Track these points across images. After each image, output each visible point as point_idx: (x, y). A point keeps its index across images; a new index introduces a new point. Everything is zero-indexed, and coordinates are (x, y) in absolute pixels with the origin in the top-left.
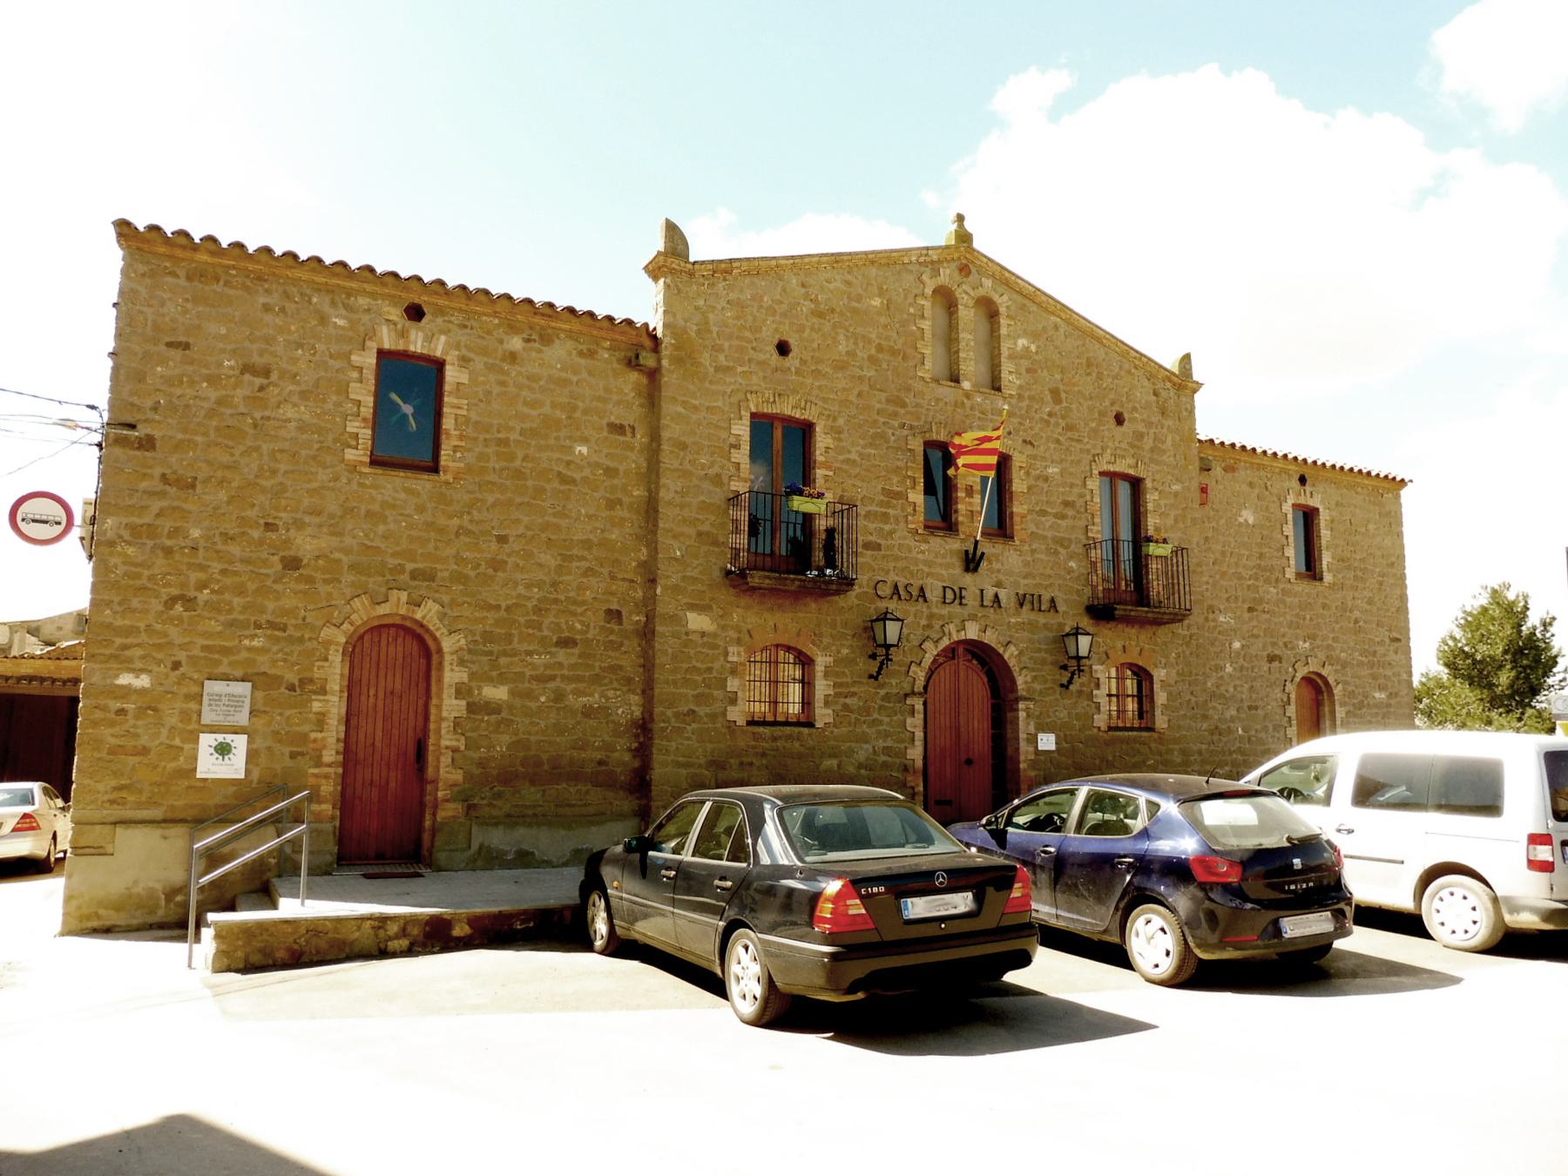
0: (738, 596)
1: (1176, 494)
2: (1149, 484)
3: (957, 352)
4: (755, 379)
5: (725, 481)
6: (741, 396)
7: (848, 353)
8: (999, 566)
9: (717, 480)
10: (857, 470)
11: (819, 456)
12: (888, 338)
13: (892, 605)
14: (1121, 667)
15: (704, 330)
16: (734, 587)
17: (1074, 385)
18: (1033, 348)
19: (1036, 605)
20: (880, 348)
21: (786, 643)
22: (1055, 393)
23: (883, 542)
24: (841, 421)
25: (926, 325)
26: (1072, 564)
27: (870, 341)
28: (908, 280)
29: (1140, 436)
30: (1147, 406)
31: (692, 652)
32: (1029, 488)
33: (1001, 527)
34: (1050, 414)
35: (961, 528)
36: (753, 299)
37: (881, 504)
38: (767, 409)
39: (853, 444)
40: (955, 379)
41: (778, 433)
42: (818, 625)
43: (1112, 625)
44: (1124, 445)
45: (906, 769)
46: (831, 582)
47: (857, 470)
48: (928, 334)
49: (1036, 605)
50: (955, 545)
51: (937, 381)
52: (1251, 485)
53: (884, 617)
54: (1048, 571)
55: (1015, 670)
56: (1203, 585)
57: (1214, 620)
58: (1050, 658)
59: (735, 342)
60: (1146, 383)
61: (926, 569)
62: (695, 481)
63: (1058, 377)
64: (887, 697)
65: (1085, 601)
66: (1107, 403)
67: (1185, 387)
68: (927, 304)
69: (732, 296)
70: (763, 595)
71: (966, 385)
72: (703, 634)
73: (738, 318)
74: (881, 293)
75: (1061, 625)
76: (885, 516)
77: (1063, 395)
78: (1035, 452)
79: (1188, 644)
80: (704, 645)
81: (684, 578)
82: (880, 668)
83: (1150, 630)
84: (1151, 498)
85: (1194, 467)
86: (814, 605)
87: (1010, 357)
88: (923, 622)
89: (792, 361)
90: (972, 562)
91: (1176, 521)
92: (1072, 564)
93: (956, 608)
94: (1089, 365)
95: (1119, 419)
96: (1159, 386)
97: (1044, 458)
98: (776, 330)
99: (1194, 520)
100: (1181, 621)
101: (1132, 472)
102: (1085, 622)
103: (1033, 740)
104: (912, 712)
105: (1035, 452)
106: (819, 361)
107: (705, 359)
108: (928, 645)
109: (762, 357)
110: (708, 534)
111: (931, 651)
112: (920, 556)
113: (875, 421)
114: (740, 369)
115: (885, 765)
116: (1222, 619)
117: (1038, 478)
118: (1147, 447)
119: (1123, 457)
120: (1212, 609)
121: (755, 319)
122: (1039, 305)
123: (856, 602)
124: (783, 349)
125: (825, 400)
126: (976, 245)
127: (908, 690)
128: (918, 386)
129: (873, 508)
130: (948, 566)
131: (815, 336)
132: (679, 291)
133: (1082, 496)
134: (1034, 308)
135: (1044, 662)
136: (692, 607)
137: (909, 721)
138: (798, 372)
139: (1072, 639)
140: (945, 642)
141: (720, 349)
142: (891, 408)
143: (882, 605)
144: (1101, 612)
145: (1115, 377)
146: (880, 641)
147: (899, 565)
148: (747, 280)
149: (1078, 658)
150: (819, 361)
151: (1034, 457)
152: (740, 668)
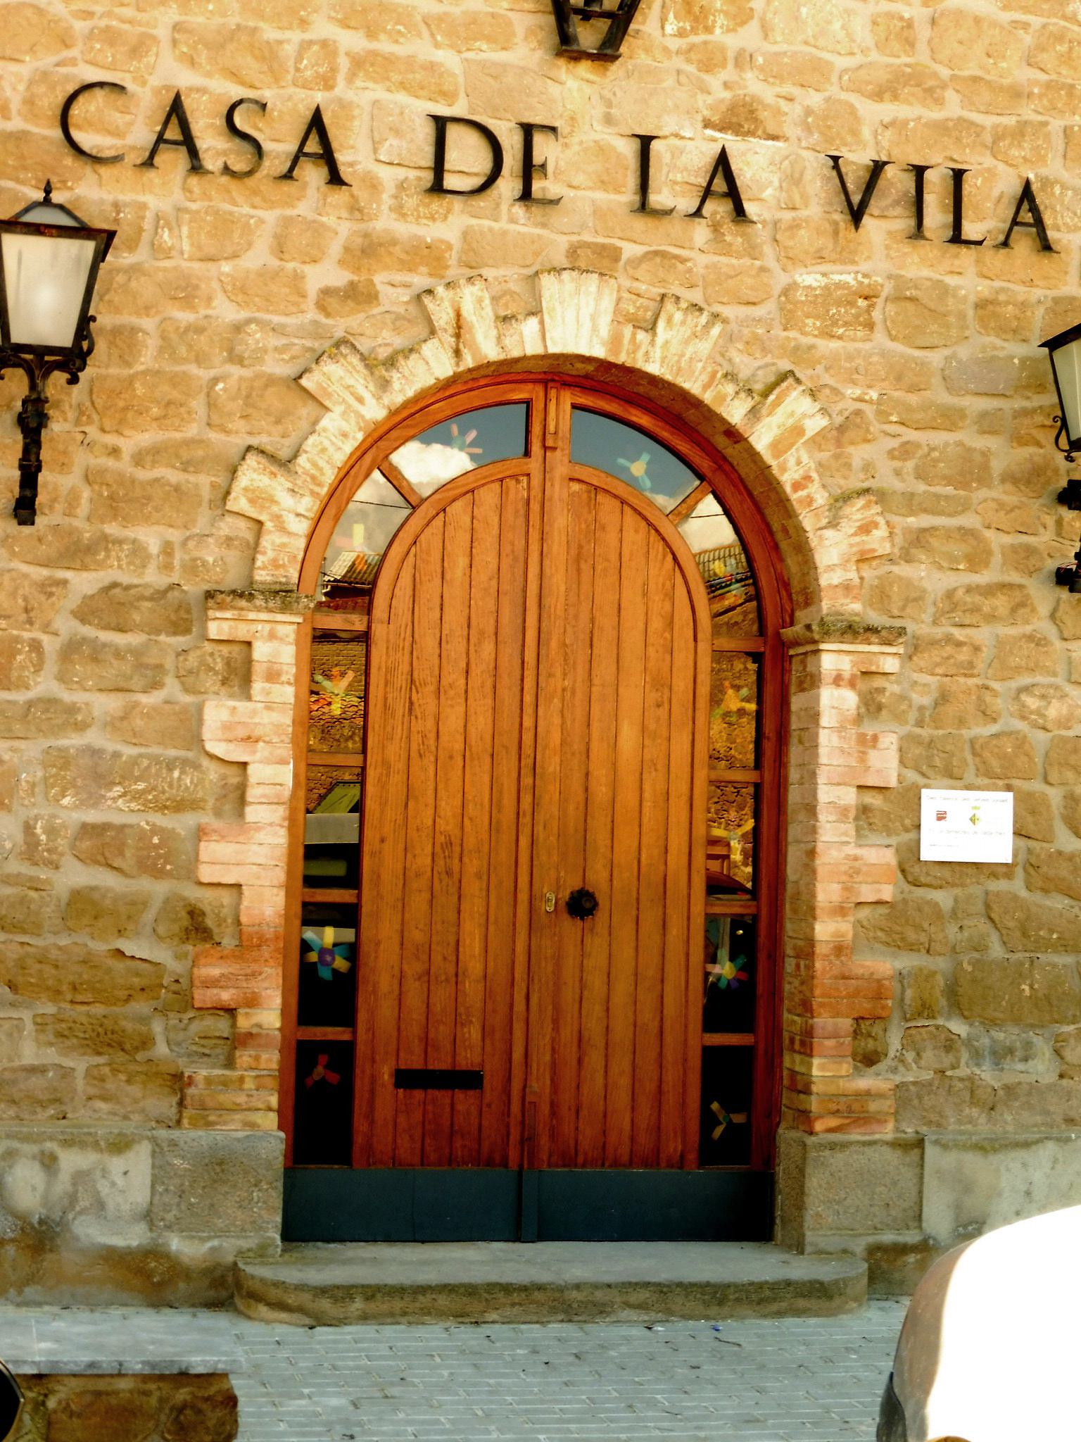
8: (748, 37)
19: (936, 215)
45: (196, 927)
49: (936, 215)
58: (1004, 455)
64: (110, 607)
88: (326, 274)
93: (503, 213)
103: (891, 812)
104: (240, 673)
108: (338, 377)
115: (83, 907)
135: (972, 471)
137: (218, 712)
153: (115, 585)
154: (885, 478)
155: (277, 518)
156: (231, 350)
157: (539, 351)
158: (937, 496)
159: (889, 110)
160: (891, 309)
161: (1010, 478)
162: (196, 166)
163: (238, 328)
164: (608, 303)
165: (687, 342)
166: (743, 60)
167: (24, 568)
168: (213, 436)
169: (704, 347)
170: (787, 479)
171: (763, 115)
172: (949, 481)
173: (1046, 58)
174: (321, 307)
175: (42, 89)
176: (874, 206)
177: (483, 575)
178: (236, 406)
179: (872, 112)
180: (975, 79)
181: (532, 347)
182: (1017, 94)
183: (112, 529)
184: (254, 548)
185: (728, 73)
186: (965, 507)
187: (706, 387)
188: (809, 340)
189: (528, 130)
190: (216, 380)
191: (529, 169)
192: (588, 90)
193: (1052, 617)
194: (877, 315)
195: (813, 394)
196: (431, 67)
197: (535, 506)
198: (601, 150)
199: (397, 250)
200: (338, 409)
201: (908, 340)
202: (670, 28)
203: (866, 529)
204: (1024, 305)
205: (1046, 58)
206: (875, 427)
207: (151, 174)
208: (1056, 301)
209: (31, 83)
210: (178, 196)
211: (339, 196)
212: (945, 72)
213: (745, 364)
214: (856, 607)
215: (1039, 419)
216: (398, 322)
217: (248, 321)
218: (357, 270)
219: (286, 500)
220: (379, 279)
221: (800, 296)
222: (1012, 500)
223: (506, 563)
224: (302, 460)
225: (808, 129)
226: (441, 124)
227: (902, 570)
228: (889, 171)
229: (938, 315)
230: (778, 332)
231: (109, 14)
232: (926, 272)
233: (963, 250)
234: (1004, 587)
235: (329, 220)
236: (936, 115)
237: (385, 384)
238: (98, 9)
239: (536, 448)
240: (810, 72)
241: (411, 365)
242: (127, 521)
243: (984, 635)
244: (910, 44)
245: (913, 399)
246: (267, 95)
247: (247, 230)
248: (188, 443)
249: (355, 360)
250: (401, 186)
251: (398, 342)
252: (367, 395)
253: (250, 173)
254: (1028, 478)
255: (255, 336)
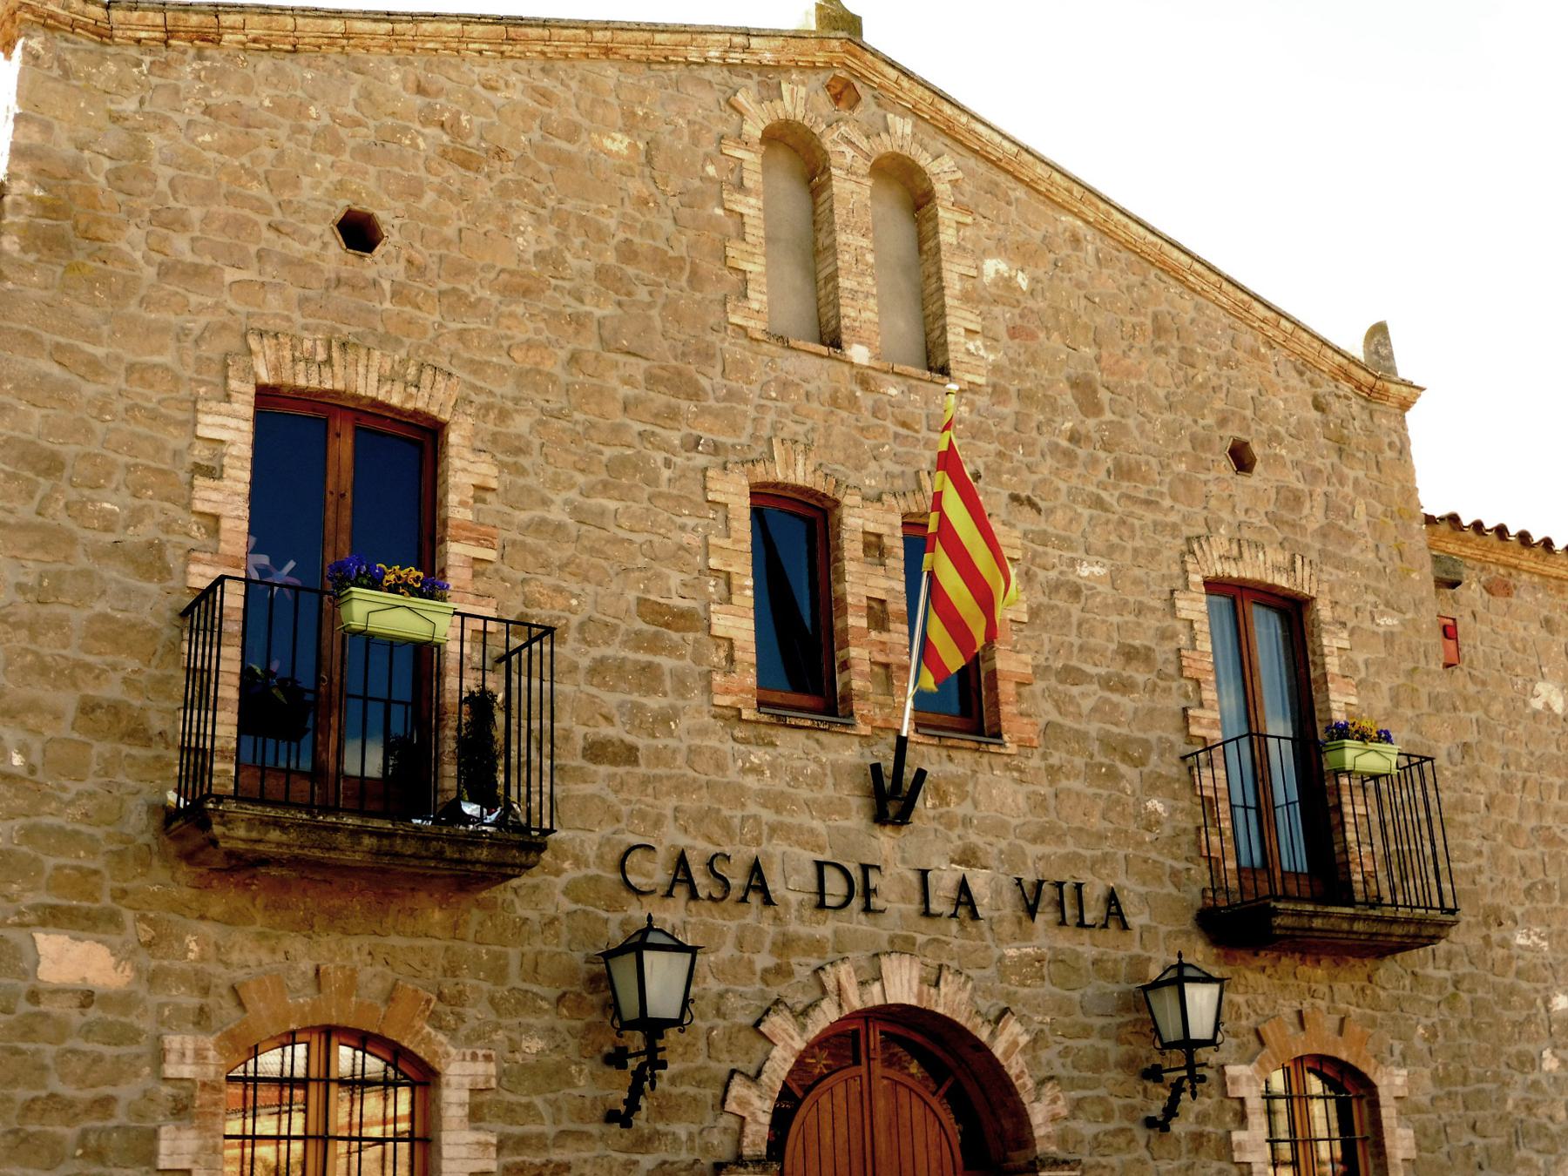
0: (203, 886)
1: (1389, 638)
2: (1324, 611)
3: (833, 277)
4: (274, 302)
5: (174, 562)
6: (232, 342)
7: (540, 257)
8: (966, 809)
9: (151, 560)
10: (569, 550)
11: (457, 506)
12: (648, 230)
13: (672, 915)
14: (1299, 1065)
15: (131, 167)
16: (189, 857)
17: (1128, 373)
18: (1023, 281)
20: (628, 253)
21: (352, 1023)
22: (1083, 388)
23: (642, 742)
24: (521, 424)
25: (750, 206)
26: (1156, 805)
27: (601, 234)
28: (701, 102)
29: (1294, 500)
30: (1301, 433)
31: (49, 1051)
32: (1034, 613)
33: (967, 706)
34: (1074, 437)
35: (858, 706)
36: (278, 107)
37: (637, 641)
38: (305, 379)
39: (555, 483)
40: (832, 340)
41: (342, 449)
42: (452, 970)
43: (1265, 959)
44: (1258, 520)
46: (475, 839)
47: (569, 550)
48: (755, 232)
50: (846, 753)
51: (782, 340)
52: (1547, 623)
53: (639, 943)
54: (1096, 823)
55: (1025, 1085)
56: (1479, 858)
57: (1505, 944)
58: (1115, 1051)
59: (223, 209)
60: (1294, 380)
61: (768, 815)
62: (83, 562)
63: (1088, 352)
65: (1193, 896)
66: (1210, 420)
67: (1384, 394)
68: (752, 159)
69: (218, 97)
70: (284, 884)
71: (859, 353)
72: (87, 998)
73: (233, 149)
74: (630, 125)
75: (1139, 963)
76: (648, 677)
77: (1104, 396)
78: (1041, 524)
79: (1452, 1001)
80: (87, 1031)
81: (29, 834)
82: (636, 1091)
83: (1360, 968)
84: (1333, 645)
85: (1422, 577)
86: (437, 916)
87: (966, 297)
88: (764, 960)
89: (382, 264)
90: (892, 798)
91: (1396, 701)
92: (1156, 805)
93: (854, 921)
94: (1159, 330)
95: (1241, 458)
96: (1326, 388)
97: (1065, 543)
98: (341, 186)
99: (1433, 699)
100: (1433, 939)
101: (1281, 581)
102: (1200, 954)
105: (1041, 524)
106: (461, 270)
107: (132, 242)
108: (778, 1024)
109: (296, 248)
110: (115, 709)
111: (788, 1043)
112: (750, 781)
113: (617, 429)
114: (230, 275)
116: (1520, 940)
117: (1054, 588)
118: (1313, 526)
119: (1258, 546)
120: (1494, 917)
121: (280, 157)
122: (1030, 186)
123: (567, 905)
124: (359, 232)
125: (477, 367)
126: (871, 36)
127: (725, 1153)
128: (731, 347)
129: (614, 651)
130: (827, 809)
131: (451, 209)
132: (67, 73)
133: (1165, 635)
134: (1020, 192)
135: (1099, 1063)
136: (53, 918)
138: (398, 294)
139: (1169, 994)
140: (827, 1015)
141: (178, 223)
142: (660, 399)
143: (637, 913)
144: (1238, 926)
145: (1224, 362)
146: (630, 1009)
147: (690, 803)
148: (265, 64)
149: (1188, 1045)
150: (461, 270)
151: (1043, 538)
152: (201, 1098)
153: (664, 1163)
154: (1058, 1070)
155: (753, 1114)
156: (718, 1010)
157: (882, 1002)
158: (1085, 1079)
159: (1039, 849)
160: (1052, 967)
161: (1118, 1065)
162: (693, 895)
163: (721, 996)
164: (916, 973)
165: (955, 993)
166: (967, 822)
167: (614, 1154)
168: (712, 1064)
169: (965, 996)
170: (1012, 1072)
171: (980, 854)
172: (1089, 1068)
173: (1112, 815)
174: (764, 980)
175: (607, 849)
176: (1041, 905)
177: (840, 1141)
178: (723, 1045)
179: (1033, 850)
180: (1080, 829)
181: (878, 1001)
182: (1101, 837)
183: (660, 1126)
184: (741, 1132)
185: (958, 830)
186: (1098, 1084)
187: (968, 1019)
188: (1012, 989)
189: (865, 868)
190: (712, 1029)
191: (868, 892)
192: (892, 842)
193: (1147, 1146)
194: (1045, 971)
195: (1020, 1021)
196: (812, 831)
197: (866, 1096)
198: (902, 878)
199: (802, 943)
200: (780, 1044)
201: (1062, 986)
202: (929, 804)
203: (1054, 1101)
204: (1115, 961)
205: (1112, 815)
206: (1051, 1039)
207: (669, 901)
208: (1131, 958)
209: (600, 845)
210: (682, 914)
211: (769, 912)
212: (1065, 826)
213: (983, 1005)
214: (1053, 1148)
215: (1130, 1028)
216: (805, 989)
217: (727, 991)
218: (780, 956)
219: (757, 1103)
220: (793, 961)
221: (1007, 962)
222: (1121, 1077)
223: (853, 1131)
224: (764, 1077)
225: (1002, 862)
226: (820, 866)
227: (1072, 1124)
228: (1045, 886)
229: (1076, 970)
230: (998, 985)
231: (639, 801)
232: (1067, 945)
233: (1086, 932)
234: (1122, 1130)
235: (764, 926)
236: (1062, 851)
237: (804, 1027)
238: (634, 798)
239: (864, 1060)
240: (1000, 829)
241: (816, 1014)
242: (668, 1121)
243: (1114, 1160)
244: (1046, 809)
245: (1067, 1020)
246: (727, 850)
247: (722, 934)
248: (699, 1069)
249: (787, 1013)
250: (801, 904)
251: (807, 1000)
252: (795, 1034)
253: (723, 899)
254: (1128, 1064)
255: (732, 1000)
